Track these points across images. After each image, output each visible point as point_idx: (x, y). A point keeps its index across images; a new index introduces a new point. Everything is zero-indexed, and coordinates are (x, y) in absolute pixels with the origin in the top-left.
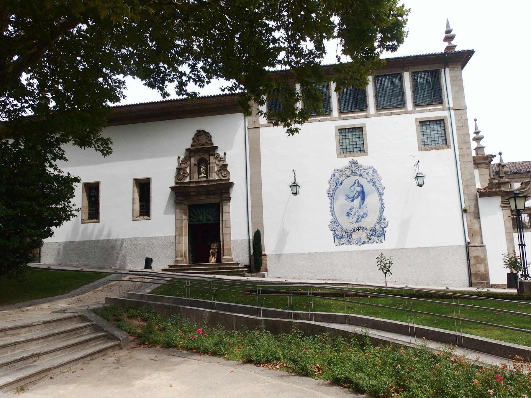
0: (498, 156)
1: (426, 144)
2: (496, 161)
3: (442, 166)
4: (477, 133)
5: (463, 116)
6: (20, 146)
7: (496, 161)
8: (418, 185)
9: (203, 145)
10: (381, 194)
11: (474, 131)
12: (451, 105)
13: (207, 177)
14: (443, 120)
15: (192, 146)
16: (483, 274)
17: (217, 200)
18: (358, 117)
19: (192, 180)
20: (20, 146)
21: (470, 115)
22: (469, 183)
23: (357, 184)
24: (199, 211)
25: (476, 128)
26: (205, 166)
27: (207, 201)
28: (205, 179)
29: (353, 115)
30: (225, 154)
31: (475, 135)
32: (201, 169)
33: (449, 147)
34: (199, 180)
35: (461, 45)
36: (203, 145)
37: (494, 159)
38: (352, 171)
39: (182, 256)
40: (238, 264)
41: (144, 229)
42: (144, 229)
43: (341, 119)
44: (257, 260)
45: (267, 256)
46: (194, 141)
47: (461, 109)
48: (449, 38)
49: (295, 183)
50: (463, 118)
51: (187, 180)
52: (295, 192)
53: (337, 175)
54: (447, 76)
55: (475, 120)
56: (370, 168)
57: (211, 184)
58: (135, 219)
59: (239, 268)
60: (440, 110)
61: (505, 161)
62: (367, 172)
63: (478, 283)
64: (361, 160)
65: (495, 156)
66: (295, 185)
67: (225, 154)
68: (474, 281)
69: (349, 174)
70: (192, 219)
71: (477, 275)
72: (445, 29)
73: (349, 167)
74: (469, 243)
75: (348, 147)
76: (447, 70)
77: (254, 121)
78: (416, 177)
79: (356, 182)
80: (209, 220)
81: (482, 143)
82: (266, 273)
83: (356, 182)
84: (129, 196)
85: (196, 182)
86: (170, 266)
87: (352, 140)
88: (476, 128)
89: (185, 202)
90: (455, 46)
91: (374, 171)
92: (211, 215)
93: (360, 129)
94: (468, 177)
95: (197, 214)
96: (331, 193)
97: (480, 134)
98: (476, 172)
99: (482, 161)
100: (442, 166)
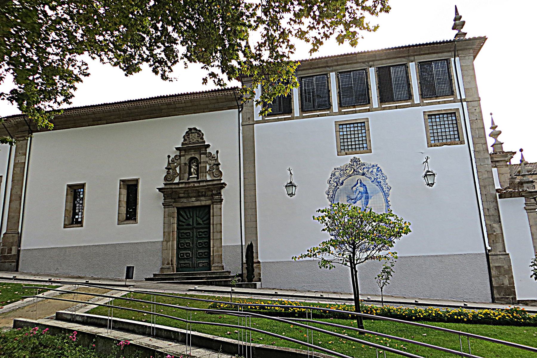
0: (519, 154)
1: (436, 140)
2: (516, 160)
3: (455, 162)
4: (494, 127)
5: (477, 108)
6: (16, 30)
7: (516, 160)
8: (428, 184)
9: (194, 143)
10: (386, 195)
11: (491, 126)
12: (463, 97)
13: (198, 178)
14: (455, 113)
15: (183, 144)
16: (508, 288)
17: (208, 202)
18: (360, 111)
19: (181, 181)
20: (16, 30)
21: (486, 108)
22: (486, 183)
23: (359, 184)
24: (188, 215)
25: (493, 123)
26: (196, 166)
27: (198, 204)
28: (195, 180)
29: (354, 109)
30: (217, 152)
31: (492, 130)
32: (192, 170)
33: (462, 143)
34: (189, 181)
35: (471, 31)
36: (194, 143)
37: (515, 156)
38: (354, 170)
39: (168, 264)
40: (230, 272)
41: (130, 234)
42: (130, 234)
43: (340, 113)
44: (250, 274)
45: (261, 264)
46: (185, 140)
47: (474, 101)
48: (458, 23)
49: (291, 183)
50: (478, 111)
51: (177, 180)
52: (291, 193)
53: (337, 174)
54: (457, 65)
55: (491, 114)
56: (373, 166)
57: (201, 184)
58: (120, 222)
59: (229, 277)
60: (450, 102)
61: (529, 159)
62: (370, 171)
63: (502, 298)
64: (362, 157)
65: (515, 153)
66: (291, 185)
67: (217, 152)
68: (496, 296)
69: (351, 173)
70: (180, 223)
71: (500, 288)
72: (453, 16)
73: (351, 166)
74: (489, 250)
75: (349, 137)
76: (457, 59)
77: (248, 117)
78: (426, 175)
79: (359, 182)
80: (200, 224)
81: (500, 139)
82: (258, 284)
83: (359, 182)
84: (115, 197)
85: (186, 183)
86: (155, 275)
87: (354, 139)
88: (493, 123)
89: (174, 205)
90: (466, 34)
91: (379, 170)
92: (201, 219)
93: (363, 124)
94: (485, 176)
95: (186, 218)
96: (331, 193)
97: (497, 129)
98: (495, 170)
99: (500, 157)
100: (455, 162)
